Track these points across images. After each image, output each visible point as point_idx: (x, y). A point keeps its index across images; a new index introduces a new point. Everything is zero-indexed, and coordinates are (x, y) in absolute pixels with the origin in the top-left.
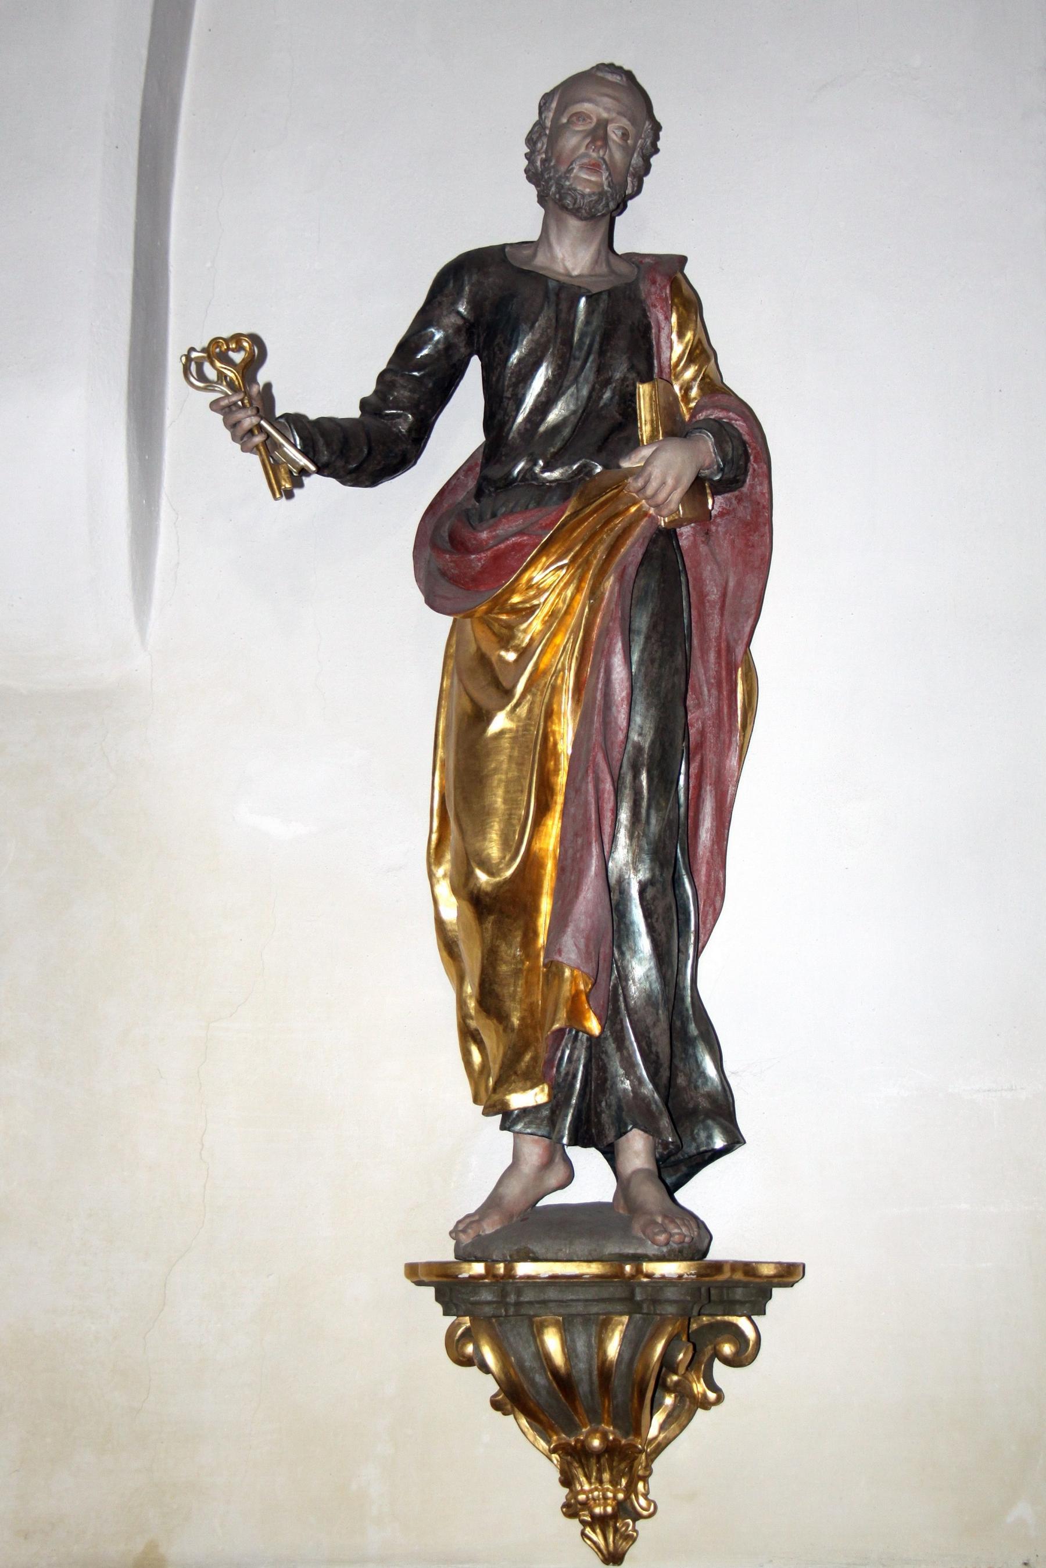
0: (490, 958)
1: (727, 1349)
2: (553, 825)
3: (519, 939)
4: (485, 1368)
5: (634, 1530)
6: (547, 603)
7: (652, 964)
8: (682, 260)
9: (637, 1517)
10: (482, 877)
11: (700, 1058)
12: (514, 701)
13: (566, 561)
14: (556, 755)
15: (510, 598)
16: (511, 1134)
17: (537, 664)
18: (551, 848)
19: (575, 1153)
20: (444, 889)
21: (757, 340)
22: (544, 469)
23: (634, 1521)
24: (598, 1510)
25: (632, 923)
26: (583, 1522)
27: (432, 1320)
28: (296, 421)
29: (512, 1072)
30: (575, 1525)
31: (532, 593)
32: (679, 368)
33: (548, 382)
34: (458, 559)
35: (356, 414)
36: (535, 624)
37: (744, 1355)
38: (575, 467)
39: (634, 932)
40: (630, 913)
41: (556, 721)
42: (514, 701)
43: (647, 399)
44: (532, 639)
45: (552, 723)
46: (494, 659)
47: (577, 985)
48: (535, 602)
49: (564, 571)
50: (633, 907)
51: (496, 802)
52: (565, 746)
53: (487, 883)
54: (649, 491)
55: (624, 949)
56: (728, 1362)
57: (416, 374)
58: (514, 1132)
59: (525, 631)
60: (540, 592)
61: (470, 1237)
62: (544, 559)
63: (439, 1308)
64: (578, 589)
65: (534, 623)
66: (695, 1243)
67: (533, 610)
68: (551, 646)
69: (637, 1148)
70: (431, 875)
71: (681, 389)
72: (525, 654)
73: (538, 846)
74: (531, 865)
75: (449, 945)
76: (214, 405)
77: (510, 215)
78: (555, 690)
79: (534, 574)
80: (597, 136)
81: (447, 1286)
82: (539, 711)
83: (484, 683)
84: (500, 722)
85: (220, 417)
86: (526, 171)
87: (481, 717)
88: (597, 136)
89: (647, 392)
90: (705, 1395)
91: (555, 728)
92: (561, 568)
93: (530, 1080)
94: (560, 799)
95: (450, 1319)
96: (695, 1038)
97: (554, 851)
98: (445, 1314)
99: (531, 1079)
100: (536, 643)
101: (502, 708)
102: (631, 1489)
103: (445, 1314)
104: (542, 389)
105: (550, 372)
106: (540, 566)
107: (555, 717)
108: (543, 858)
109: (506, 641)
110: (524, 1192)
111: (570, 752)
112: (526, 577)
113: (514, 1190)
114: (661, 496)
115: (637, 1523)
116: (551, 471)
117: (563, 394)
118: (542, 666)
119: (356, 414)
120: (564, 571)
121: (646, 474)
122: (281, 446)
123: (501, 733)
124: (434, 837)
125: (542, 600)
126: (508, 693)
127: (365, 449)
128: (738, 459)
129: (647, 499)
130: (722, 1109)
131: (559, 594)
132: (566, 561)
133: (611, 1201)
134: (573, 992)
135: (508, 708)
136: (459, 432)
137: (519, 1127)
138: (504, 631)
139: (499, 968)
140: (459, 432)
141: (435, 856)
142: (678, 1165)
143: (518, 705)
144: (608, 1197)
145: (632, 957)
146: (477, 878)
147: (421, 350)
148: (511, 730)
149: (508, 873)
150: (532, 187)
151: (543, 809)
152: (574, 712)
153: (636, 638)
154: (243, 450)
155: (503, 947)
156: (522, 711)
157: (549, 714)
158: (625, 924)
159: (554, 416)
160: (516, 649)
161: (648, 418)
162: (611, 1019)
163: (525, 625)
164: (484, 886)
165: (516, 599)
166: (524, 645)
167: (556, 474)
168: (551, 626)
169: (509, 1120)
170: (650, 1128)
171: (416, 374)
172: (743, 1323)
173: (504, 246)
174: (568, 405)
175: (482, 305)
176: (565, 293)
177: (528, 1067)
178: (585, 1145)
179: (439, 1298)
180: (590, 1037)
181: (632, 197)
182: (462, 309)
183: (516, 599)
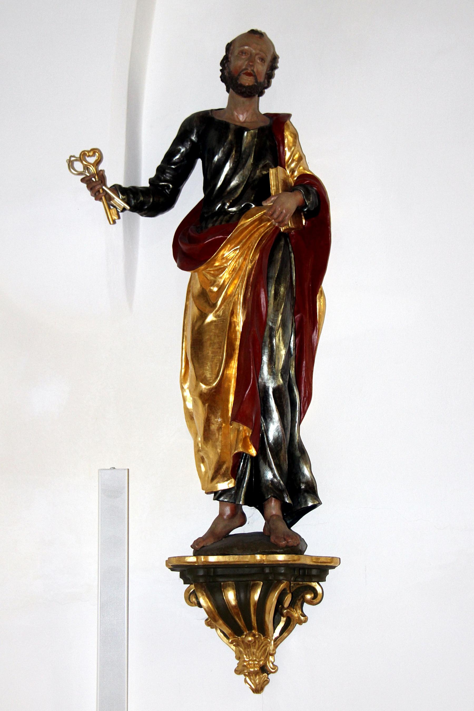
0: (208, 422)
1: (308, 597)
2: (234, 364)
3: (219, 414)
4: (200, 606)
5: (268, 678)
6: (231, 265)
7: (279, 424)
8: (289, 116)
9: (268, 673)
10: (203, 386)
11: (301, 467)
12: (217, 309)
13: (238, 247)
14: (235, 332)
15: (214, 263)
16: (218, 502)
17: (226, 292)
18: (233, 373)
19: (247, 509)
20: (187, 393)
21: (319, 148)
22: (229, 207)
23: (268, 674)
24: (252, 670)
25: (270, 406)
26: (245, 675)
27: (177, 585)
28: (117, 189)
29: (217, 474)
30: (242, 677)
31: (224, 261)
32: (289, 163)
33: (231, 169)
34: (193, 248)
35: (148, 185)
36: (225, 275)
37: (317, 599)
38: (243, 206)
39: (271, 410)
40: (270, 403)
41: (196, 316)
42: (217, 309)
43: (274, 175)
44: (224, 281)
45: (233, 318)
46: (207, 291)
47: (245, 433)
48: (226, 265)
49: (238, 251)
50: (270, 399)
51: (208, 353)
52: (239, 328)
53: (205, 388)
54: (275, 216)
55: (267, 418)
56: (311, 603)
57: (173, 167)
58: (219, 501)
59: (221, 278)
60: (228, 260)
61: (200, 548)
62: (229, 246)
63: (182, 581)
64: (245, 259)
65: (225, 274)
66: (297, 547)
67: (224, 268)
68: (233, 284)
69: (274, 507)
70: (182, 388)
71: (290, 172)
72: (221, 288)
73: (228, 372)
74: (224, 379)
75: (190, 416)
76: (82, 180)
77: (216, 97)
78: (235, 304)
79: (225, 252)
80: (249, 63)
81: (187, 572)
82: (228, 313)
83: (203, 301)
84: (210, 318)
85: (85, 185)
86: (221, 77)
87: (203, 316)
88: (249, 63)
89: (274, 172)
90: (299, 618)
91: (235, 320)
92: (237, 249)
93: (225, 477)
94: (237, 352)
95: (188, 586)
96: (299, 457)
97: (235, 374)
98: (184, 584)
99: (226, 477)
100: (226, 283)
101: (211, 312)
102: (267, 658)
103: (184, 584)
104: (228, 172)
105: (231, 165)
106: (227, 249)
107: (234, 315)
108: (230, 378)
109: (213, 283)
110: (225, 527)
111: (241, 330)
112: (221, 253)
113: (220, 527)
114: (280, 219)
115: (269, 675)
116: (232, 207)
117: (238, 174)
118: (229, 293)
119: (148, 185)
120: (238, 251)
121: (274, 208)
122: (114, 198)
123: (212, 322)
124: (183, 371)
125: (229, 264)
126: (214, 305)
127: (150, 199)
128: (313, 201)
129: (274, 219)
130: (312, 489)
131: (236, 261)
132: (238, 247)
133: (262, 531)
134: (244, 436)
135: (214, 312)
136: (192, 192)
137: (221, 499)
138: (212, 278)
139: (211, 427)
140: (192, 192)
141: (184, 379)
142: (294, 513)
143: (217, 311)
144: (260, 528)
145: (270, 421)
146: (201, 387)
147: (175, 156)
148: (215, 321)
149: (214, 384)
150: (223, 84)
151: (230, 357)
152: (243, 313)
153: (270, 280)
154: (96, 199)
155: (213, 417)
156: (220, 313)
157: (233, 313)
158: (267, 406)
159: (234, 183)
160: (217, 286)
161: (275, 184)
162: (261, 448)
163: (221, 275)
164: (203, 389)
165: (217, 264)
166: (221, 284)
167: (234, 209)
168: (232, 275)
169: (218, 495)
170: (280, 498)
171: (173, 167)
172: (315, 584)
173: (212, 110)
174: (239, 179)
175: (202, 136)
176: (240, 131)
177: (225, 471)
178: (250, 506)
179: (181, 576)
180: (252, 457)
181: (267, 88)
182: (193, 138)
183: (217, 264)
